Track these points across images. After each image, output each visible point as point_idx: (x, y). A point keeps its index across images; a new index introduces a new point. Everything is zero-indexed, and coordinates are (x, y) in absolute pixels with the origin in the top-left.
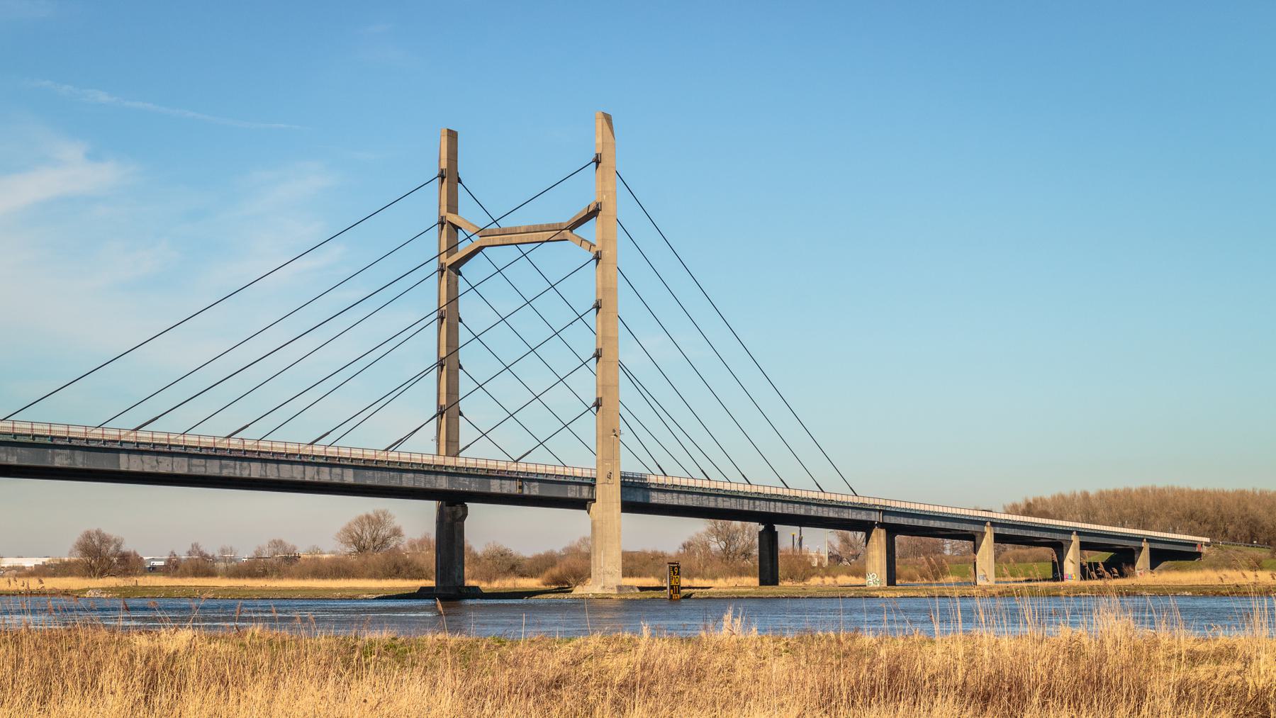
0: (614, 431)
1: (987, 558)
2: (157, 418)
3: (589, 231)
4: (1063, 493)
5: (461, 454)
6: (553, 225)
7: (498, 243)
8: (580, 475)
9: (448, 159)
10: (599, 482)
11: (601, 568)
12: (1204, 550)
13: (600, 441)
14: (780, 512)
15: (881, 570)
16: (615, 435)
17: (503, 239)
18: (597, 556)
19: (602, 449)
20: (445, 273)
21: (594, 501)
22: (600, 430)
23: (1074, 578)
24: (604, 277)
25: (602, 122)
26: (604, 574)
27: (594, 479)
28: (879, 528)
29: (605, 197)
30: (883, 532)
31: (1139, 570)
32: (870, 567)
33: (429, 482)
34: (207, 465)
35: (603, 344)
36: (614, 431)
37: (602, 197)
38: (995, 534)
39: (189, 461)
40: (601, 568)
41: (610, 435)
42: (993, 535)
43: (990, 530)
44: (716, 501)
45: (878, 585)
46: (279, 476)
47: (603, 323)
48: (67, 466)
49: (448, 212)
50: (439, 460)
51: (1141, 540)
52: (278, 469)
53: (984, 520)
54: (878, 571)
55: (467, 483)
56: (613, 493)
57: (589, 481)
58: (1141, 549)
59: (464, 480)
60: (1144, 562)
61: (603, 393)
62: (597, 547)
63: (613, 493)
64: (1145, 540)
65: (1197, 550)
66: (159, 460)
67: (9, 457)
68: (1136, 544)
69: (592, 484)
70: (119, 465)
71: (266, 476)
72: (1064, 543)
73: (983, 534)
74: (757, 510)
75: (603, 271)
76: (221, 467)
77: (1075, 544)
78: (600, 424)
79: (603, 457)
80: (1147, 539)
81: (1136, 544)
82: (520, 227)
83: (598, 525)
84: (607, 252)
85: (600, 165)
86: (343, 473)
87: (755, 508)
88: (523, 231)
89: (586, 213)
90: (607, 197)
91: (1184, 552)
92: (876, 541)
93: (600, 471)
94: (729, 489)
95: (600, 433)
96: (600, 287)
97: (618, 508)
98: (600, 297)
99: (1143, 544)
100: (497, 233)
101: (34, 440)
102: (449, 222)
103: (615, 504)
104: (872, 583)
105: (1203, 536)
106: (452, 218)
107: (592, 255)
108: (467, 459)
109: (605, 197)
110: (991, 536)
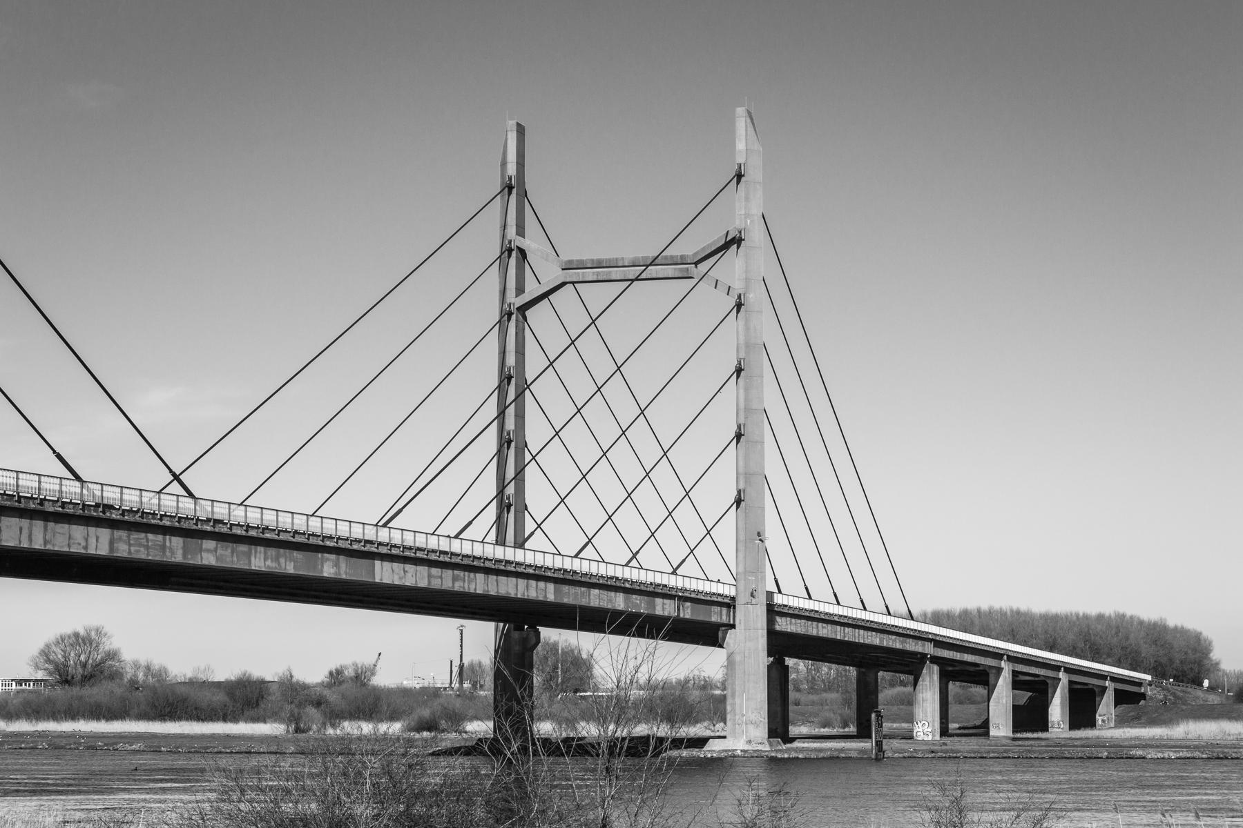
0: (759, 534)
1: (1004, 701)
2: (470, 523)
3: (732, 267)
4: (1213, 643)
5: (527, 545)
6: (610, 260)
7: (590, 279)
8: (387, 541)
9: (517, 163)
10: (739, 601)
11: (743, 715)
12: (1149, 691)
13: (742, 548)
14: (862, 642)
15: (933, 716)
16: (760, 540)
17: (598, 274)
18: (737, 700)
19: (745, 557)
20: (514, 317)
21: (733, 626)
22: (742, 533)
23: (1062, 726)
24: (747, 328)
25: (746, 122)
26: (746, 724)
27: (733, 599)
28: (931, 662)
29: (749, 221)
30: (936, 668)
31: (1100, 716)
32: (919, 712)
33: (610, 601)
34: (443, 576)
35: (746, 418)
36: (759, 534)
37: (746, 222)
38: (1013, 670)
39: (429, 569)
40: (743, 715)
41: (751, 541)
42: (1011, 673)
43: (1008, 665)
44: (924, 645)
45: (930, 738)
46: (498, 592)
47: (747, 390)
48: (333, 576)
49: (517, 234)
50: (499, 553)
51: (1056, 668)
52: (497, 580)
53: (1059, 664)
54: (930, 719)
55: (638, 602)
56: (757, 616)
57: (727, 601)
58: (1104, 689)
59: (636, 599)
60: (1108, 706)
61: (746, 482)
62: (737, 688)
63: (757, 616)
64: (1005, 657)
65: (1143, 691)
66: (406, 569)
67: (288, 563)
68: (1050, 673)
69: (730, 604)
70: (374, 578)
71: (488, 591)
72: (1049, 681)
73: (999, 670)
74: (846, 639)
75: (747, 321)
76: (455, 579)
77: (1063, 683)
78: (741, 524)
79: (745, 568)
80: (1065, 668)
81: (1050, 673)
82: (623, 259)
83: (738, 658)
84: (751, 296)
85: (743, 179)
86: (546, 588)
87: (845, 637)
88: (627, 265)
89: (723, 242)
90: (751, 221)
91: (1130, 692)
92: (928, 679)
93: (741, 587)
94: (303, 529)
95: (742, 537)
96: (742, 341)
97: (763, 636)
98: (742, 355)
99: (1107, 683)
100: (589, 265)
101: (214, 527)
102: (518, 247)
103: (760, 631)
104: (922, 734)
105: (1145, 672)
106: (520, 242)
107: (732, 301)
108: (535, 554)
109: (749, 221)
110: (1009, 673)
